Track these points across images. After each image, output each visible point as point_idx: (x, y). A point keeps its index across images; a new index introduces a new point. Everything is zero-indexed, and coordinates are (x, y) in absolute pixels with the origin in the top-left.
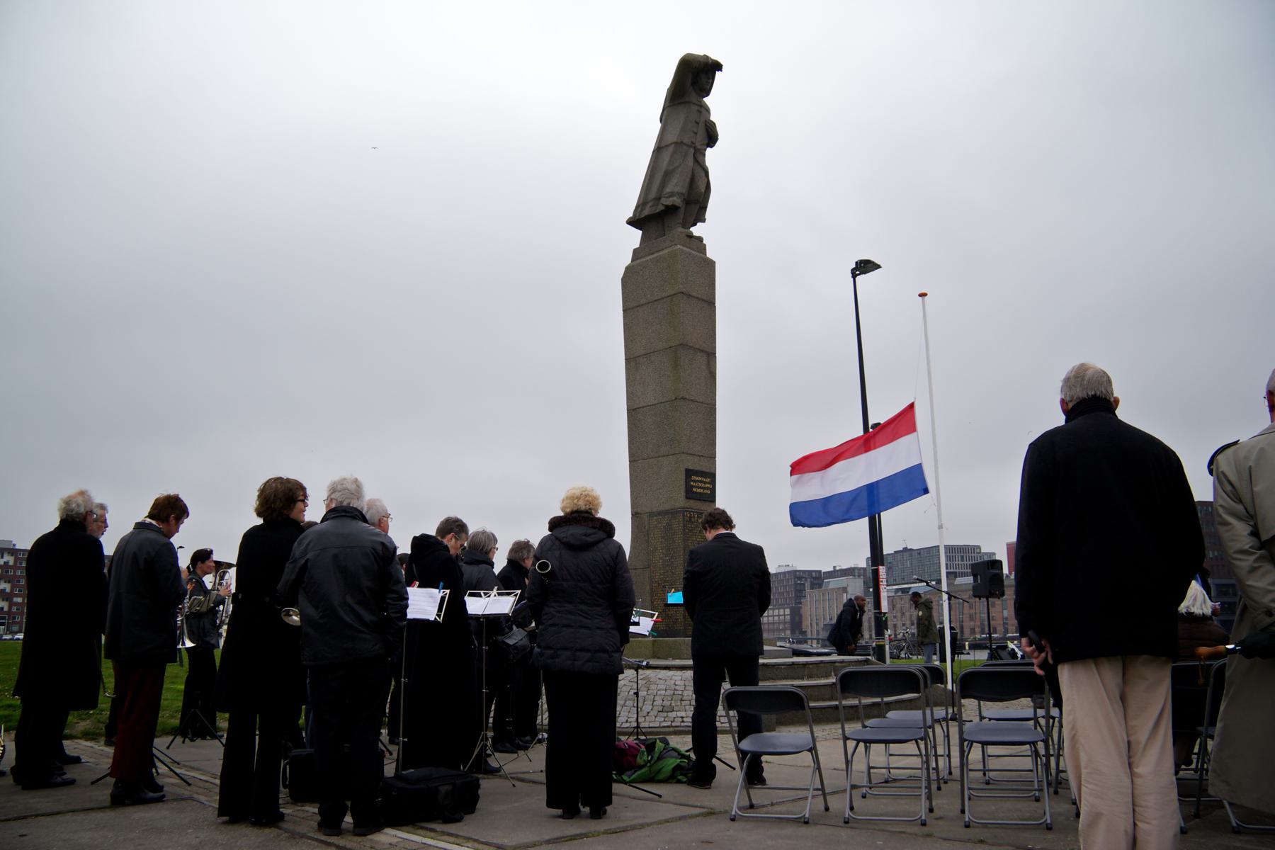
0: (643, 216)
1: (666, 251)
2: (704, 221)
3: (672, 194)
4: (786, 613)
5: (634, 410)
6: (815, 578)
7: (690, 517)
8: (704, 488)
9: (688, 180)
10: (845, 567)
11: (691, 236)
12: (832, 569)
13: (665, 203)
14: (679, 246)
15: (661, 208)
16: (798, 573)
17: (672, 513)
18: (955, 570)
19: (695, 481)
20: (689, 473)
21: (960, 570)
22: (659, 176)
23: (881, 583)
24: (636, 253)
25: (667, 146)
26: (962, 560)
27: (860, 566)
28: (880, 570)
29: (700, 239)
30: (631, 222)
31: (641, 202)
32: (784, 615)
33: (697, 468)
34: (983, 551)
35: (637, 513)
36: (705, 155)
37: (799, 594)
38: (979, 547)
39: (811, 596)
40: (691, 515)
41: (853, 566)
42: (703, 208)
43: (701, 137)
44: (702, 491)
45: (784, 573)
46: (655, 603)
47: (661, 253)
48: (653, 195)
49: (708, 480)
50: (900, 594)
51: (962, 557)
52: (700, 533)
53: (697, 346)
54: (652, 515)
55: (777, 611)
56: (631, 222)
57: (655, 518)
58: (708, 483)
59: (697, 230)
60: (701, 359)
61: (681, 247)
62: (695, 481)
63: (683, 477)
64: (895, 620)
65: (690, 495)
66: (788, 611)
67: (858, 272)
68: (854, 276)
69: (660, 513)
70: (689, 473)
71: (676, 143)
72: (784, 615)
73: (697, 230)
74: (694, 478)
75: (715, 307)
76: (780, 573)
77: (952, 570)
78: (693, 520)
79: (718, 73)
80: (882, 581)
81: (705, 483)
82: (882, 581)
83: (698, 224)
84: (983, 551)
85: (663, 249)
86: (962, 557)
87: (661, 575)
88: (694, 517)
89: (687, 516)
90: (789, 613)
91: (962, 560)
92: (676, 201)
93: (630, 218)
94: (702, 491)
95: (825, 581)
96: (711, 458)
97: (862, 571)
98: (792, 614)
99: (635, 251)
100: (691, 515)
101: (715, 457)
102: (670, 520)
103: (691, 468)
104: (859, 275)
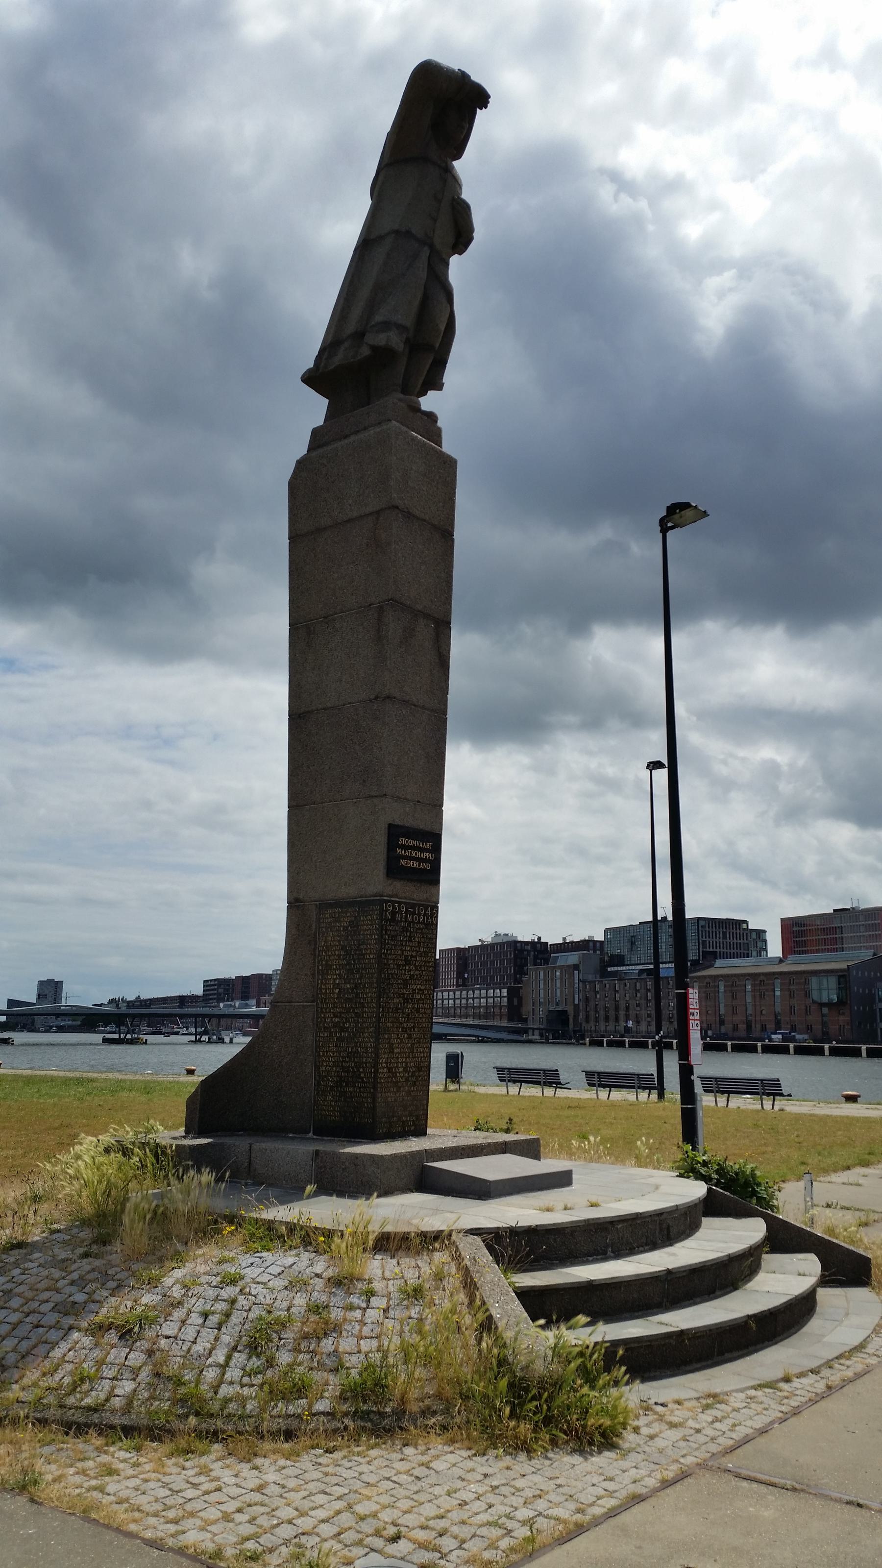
0: (332, 367)
1: (372, 432)
2: (439, 386)
3: (386, 326)
4: (502, 995)
5: (300, 716)
6: (540, 952)
7: (393, 913)
8: (420, 860)
9: (416, 303)
10: (576, 939)
11: (417, 409)
12: (561, 942)
13: (371, 343)
14: (394, 422)
15: (365, 351)
16: (518, 945)
17: (362, 905)
18: (715, 950)
19: (405, 847)
20: (395, 832)
21: (725, 950)
22: (364, 293)
23: (691, 1017)
24: (318, 438)
25: (381, 238)
26: (725, 937)
27: (596, 939)
28: (691, 996)
29: (431, 417)
30: (312, 379)
31: (329, 342)
32: (501, 997)
33: (409, 822)
34: (750, 927)
35: (297, 900)
36: (448, 265)
37: (520, 970)
38: (745, 922)
39: (536, 976)
40: (394, 907)
41: (587, 938)
42: (440, 363)
43: (443, 235)
44: (416, 864)
45: (502, 944)
46: (322, 1069)
47: (361, 436)
48: (351, 327)
49: (428, 845)
50: (644, 976)
51: (724, 934)
52: (409, 941)
53: (419, 607)
54: (324, 906)
55: (492, 991)
56: (312, 379)
57: (330, 911)
58: (427, 850)
59: (429, 402)
60: (424, 631)
61: (397, 424)
62: (405, 847)
63: (382, 839)
64: (638, 1009)
65: (394, 870)
66: (505, 992)
67: (670, 524)
68: (664, 530)
69: (337, 904)
70: (395, 832)
71: (397, 232)
72: (501, 997)
73: (429, 402)
74: (402, 841)
75: (453, 540)
76: (497, 944)
77: (711, 950)
78: (398, 917)
79: (480, 113)
80: (693, 1014)
81: (421, 850)
82: (693, 1014)
83: (430, 392)
84: (750, 927)
85: (365, 429)
86: (724, 934)
87: (335, 1016)
88: (400, 912)
89: (386, 911)
90: (506, 995)
91: (725, 937)
92: (395, 340)
93: (309, 371)
94: (416, 864)
95: (552, 955)
96: (435, 806)
97: (598, 944)
98: (510, 996)
99: (315, 432)
100: (394, 907)
101: (442, 805)
102: (355, 917)
103: (398, 822)
104: (672, 528)
